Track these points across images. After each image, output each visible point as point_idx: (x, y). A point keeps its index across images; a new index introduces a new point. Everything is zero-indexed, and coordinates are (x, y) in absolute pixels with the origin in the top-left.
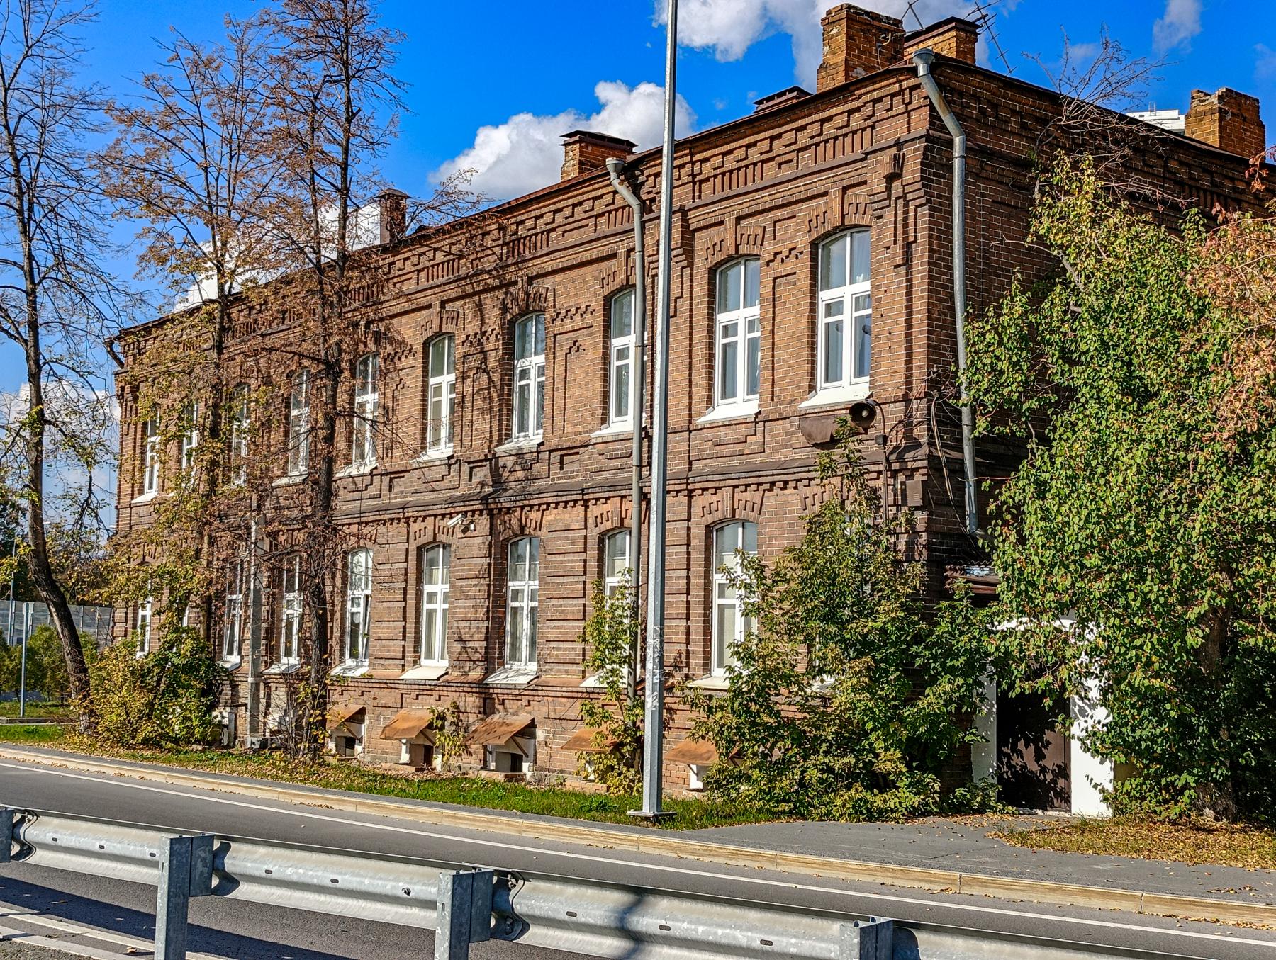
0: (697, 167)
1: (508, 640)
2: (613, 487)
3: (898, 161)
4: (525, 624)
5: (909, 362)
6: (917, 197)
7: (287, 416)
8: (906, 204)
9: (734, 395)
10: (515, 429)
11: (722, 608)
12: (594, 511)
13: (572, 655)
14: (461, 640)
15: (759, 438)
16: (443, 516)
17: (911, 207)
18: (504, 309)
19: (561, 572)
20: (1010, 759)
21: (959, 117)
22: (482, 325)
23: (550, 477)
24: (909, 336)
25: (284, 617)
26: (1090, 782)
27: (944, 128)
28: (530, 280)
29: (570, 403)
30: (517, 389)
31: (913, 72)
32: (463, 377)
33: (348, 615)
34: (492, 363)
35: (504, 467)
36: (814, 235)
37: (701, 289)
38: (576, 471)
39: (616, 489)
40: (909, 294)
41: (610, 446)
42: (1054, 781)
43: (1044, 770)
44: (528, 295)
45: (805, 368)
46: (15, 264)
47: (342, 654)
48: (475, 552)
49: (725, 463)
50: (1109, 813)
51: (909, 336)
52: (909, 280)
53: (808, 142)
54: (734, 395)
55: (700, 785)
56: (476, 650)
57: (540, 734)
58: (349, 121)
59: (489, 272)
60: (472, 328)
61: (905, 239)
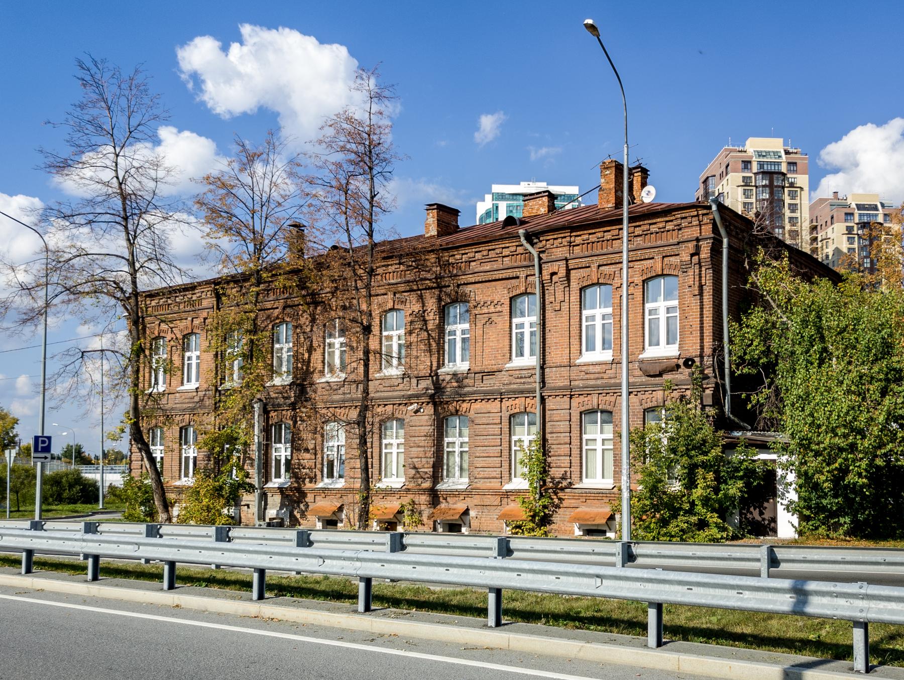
0: (572, 239)
1: (445, 467)
2: (522, 392)
3: (698, 248)
4: (458, 459)
5: (702, 339)
6: (706, 264)
7: (272, 348)
8: (700, 267)
9: (594, 349)
10: (446, 361)
11: (386, 454)
12: (506, 403)
13: (494, 474)
14: (415, 468)
15: (613, 371)
16: (400, 404)
17: (703, 269)
18: (440, 299)
19: (486, 433)
20: (746, 515)
21: (727, 228)
22: (423, 307)
23: (472, 385)
24: (702, 328)
25: (274, 458)
26: (787, 525)
27: (720, 235)
28: (458, 286)
29: (486, 351)
30: (447, 340)
31: (710, 208)
32: (410, 333)
33: (325, 456)
34: (430, 326)
35: (443, 380)
36: (645, 277)
37: (575, 297)
38: (490, 384)
39: (526, 393)
40: (702, 309)
41: (517, 372)
42: (769, 524)
43: (764, 519)
44: (457, 292)
45: (640, 339)
46: (123, 258)
47: (323, 476)
48: (425, 423)
49: (592, 383)
50: (797, 536)
51: (702, 328)
52: (702, 302)
53: (641, 233)
54: (594, 349)
55: (581, 533)
56: (426, 473)
57: (472, 513)
58: (372, 198)
59: (430, 280)
60: (417, 307)
61: (700, 283)
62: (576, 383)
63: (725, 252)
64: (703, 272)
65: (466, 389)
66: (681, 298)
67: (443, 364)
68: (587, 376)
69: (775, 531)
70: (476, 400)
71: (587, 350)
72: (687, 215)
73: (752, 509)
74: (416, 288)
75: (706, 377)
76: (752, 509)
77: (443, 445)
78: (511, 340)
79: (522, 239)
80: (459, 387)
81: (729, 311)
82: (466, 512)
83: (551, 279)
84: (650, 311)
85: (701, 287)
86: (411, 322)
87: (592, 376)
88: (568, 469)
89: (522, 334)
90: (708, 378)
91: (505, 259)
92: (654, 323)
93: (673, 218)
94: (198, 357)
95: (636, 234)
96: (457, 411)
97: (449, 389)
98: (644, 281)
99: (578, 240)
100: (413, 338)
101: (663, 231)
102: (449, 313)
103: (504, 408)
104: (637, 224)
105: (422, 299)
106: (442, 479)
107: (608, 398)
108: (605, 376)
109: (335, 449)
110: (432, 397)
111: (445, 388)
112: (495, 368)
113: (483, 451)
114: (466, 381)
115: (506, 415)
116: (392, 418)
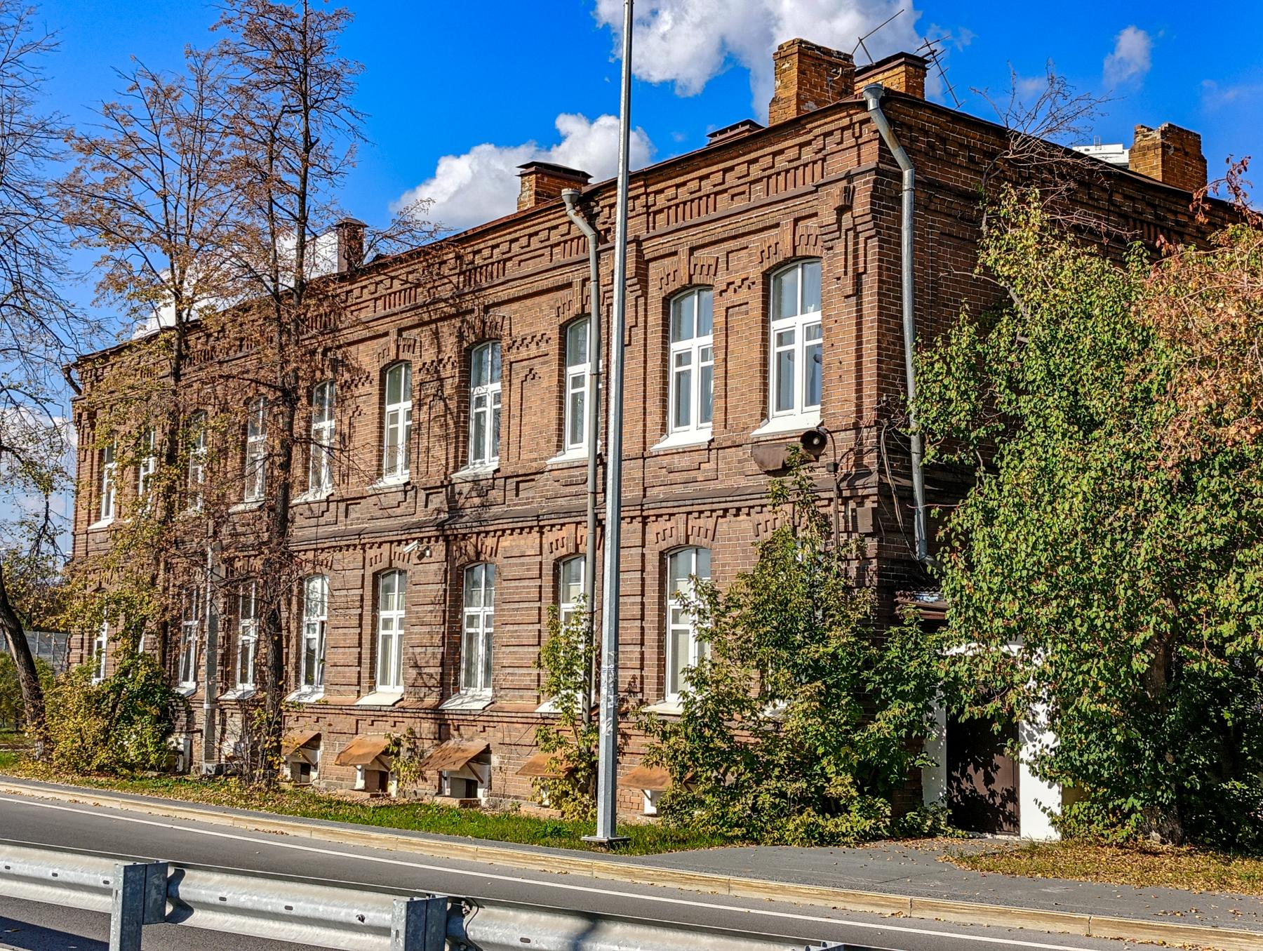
0: (651, 198)
1: (463, 666)
2: (568, 513)
3: (849, 194)
4: (481, 650)
5: (859, 390)
6: (866, 229)
8: (856, 236)
10: (471, 455)
12: (550, 537)
13: (527, 681)
14: (416, 666)
15: (712, 465)
16: (399, 542)
17: (861, 239)
18: (461, 337)
19: (517, 598)
22: (439, 352)
23: (506, 503)
24: (859, 365)
25: (240, 643)
26: (1039, 806)
27: (893, 162)
28: (487, 309)
30: (473, 417)
31: (863, 106)
33: (304, 641)
34: (448, 390)
36: (766, 266)
37: (655, 318)
38: (532, 498)
40: (859, 324)
41: (566, 473)
42: (1003, 805)
43: (993, 794)
44: (484, 323)
45: (757, 396)
47: (297, 680)
49: (678, 490)
50: (1057, 836)
51: (859, 365)
52: (859, 311)
55: (654, 810)
56: (431, 676)
57: (495, 760)
59: (445, 301)
60: (429, 356)
61: (855, 270)
62: (655, 491)
64: (861, 245)
69: (1014, 821)
70: (553, 526)
71: (779, 408)
73: (970, 769)
76: (970, 769)
83: (839, 221)
84: (679, 357)
89: (790, 355)
91: (556, 250)
92: (786, 360)
93: (810, 137)
101: (796, 166)
102: (480, 362)
105: (437, 338)
106: (457, 690)
110: (440, 526)
114: (492, 494)
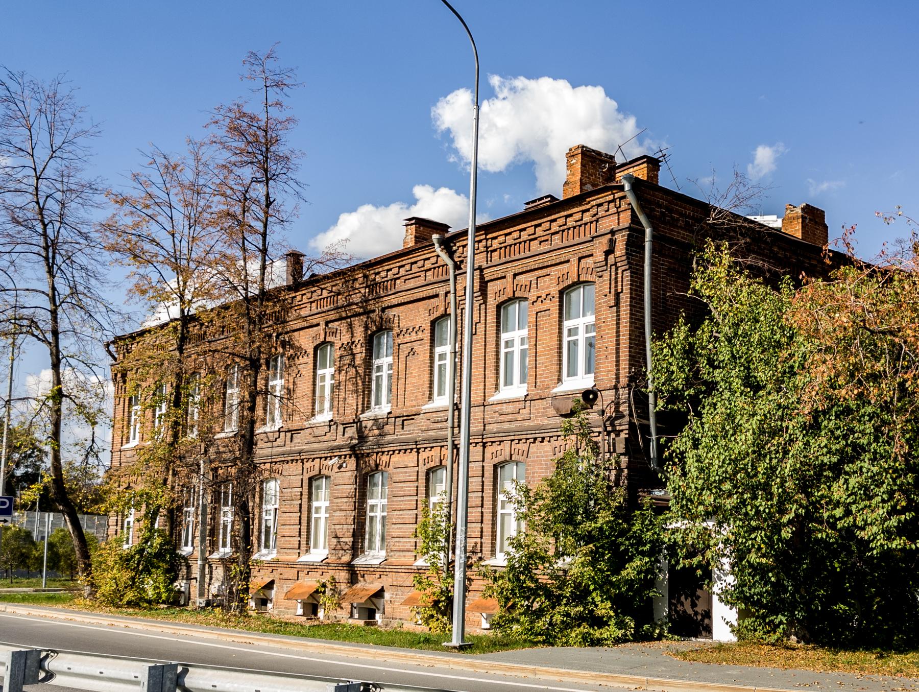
0: (489, 242)
1: (367, 536)
3: (612, 243)
6: (623, 265)
7: (224, 394)
8: (617, 269)
12: (423, 455)
14: (336, 537)
17: (620, 271)
18: (366, 328)
19: (402, 493)
20: (676, 607)
21: (649, 217)
22: (352, 337)
23: (395, 434)
24: (618, 350)
26: (724, 619)
27: (640, 224)
28: (383, 310)
30: (374, 378)
31: (622, 188)
33: (263, 522)
34: (358, 361)
35: (366, 427)
36: (561, 286)
37: (491, 318)
38: (413, 431)
40: (618, 324)
41: (434, 415)
42: (702, 620)
43: (696, 613)
44: (381, 318)
45: (555, 368)
47: (259, 546)
48: (347, 481)
49: (506, 426)
51: (618, 350)
53: (557, 229)
56: (346, 543)
57: (387, 595)
59: (357, 304)
60: (346, 339)
61: (616, 290)
63: (647, 246)
64: (620, 275)
65: (388, 438)
66: (597, 312)
67: (368, 408)
68: (502, 418)
69: (709, 630)
71: (569, 375)
72: (602, 200)
74: (345, 315)
75: (620, 416)
77: (365, 509)
78: (431, 374)
79: (437, 245)
80: (380, 435)
81: (653, 324)
82: (380, 594)
83: (606, 259)
84: (507, 342)
85: (617, 295)
86: (341, 357)
87: (506, 418)
88: (479, 540)
89: (575, 343)
90: (624, 416)
91: (429, 273)
94: (390, 367)
95: (553, 231)
96: (377, 465)
97: (371, 439)
98: (561, 293)
99: (496, 244)
100: (342, 377)
103: (421, 461)
104: (553, 217)
106: (363, 552)
107: (520, 446)
108: (519, 417)
109: (272, 513)
110: (353, 448)
111: (367, 437)
112: (414, 410)
113: (399, 517)
115: (423, 469)
116: (319, 476)
